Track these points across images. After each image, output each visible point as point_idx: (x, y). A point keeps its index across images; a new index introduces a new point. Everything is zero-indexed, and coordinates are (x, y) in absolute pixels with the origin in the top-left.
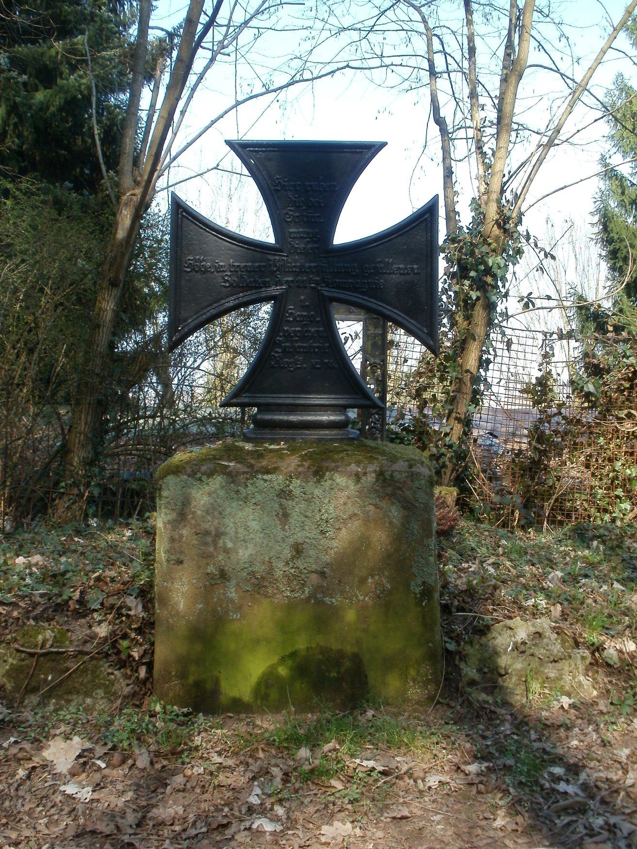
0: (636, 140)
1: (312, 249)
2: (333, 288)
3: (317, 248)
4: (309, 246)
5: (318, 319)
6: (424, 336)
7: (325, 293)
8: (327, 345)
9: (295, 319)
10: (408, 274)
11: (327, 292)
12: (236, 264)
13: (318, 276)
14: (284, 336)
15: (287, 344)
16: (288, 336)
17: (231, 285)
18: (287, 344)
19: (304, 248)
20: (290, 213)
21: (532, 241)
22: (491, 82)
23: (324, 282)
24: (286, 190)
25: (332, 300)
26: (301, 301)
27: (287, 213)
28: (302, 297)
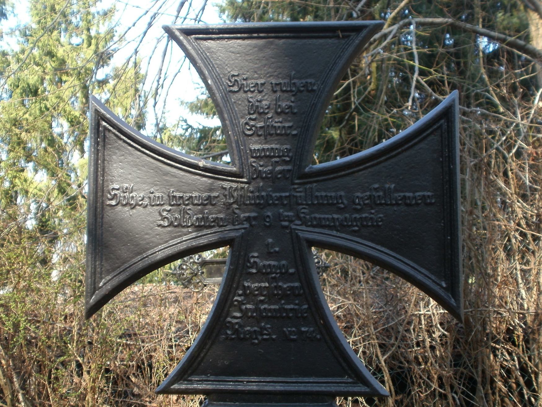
0: (541, 67)
1: (281, 172)
2: (314, 226)
3: (289, 171)
4: (279, 168)
5: (291, 271)
6: (442, 293)
7: (301, 234)
8: (306, 306)
9: (259, 271)
10: (417, 204)
11: (306, 233)
12: (178, 194)
13: (291, 210)
14: (244, 294)
15: (249, 306)
16: (249, 295)
17: (171, 224)
18: (249, 306)
19: (271, 172)
20: (252, 123)
21: (472, 153)
22: (182, 184)
23: (299, 218)
24: (246, 92)
25: (311, 243)
26: (268, 245)
27: (247, 124)
28: (270, 240)
